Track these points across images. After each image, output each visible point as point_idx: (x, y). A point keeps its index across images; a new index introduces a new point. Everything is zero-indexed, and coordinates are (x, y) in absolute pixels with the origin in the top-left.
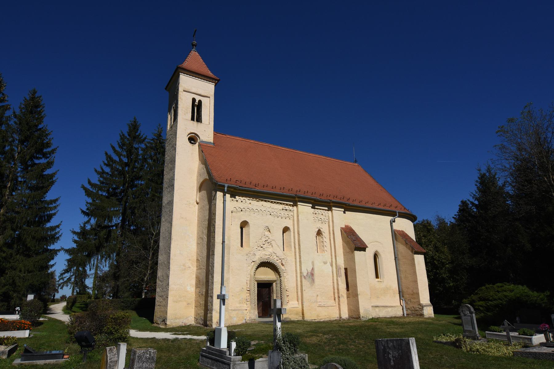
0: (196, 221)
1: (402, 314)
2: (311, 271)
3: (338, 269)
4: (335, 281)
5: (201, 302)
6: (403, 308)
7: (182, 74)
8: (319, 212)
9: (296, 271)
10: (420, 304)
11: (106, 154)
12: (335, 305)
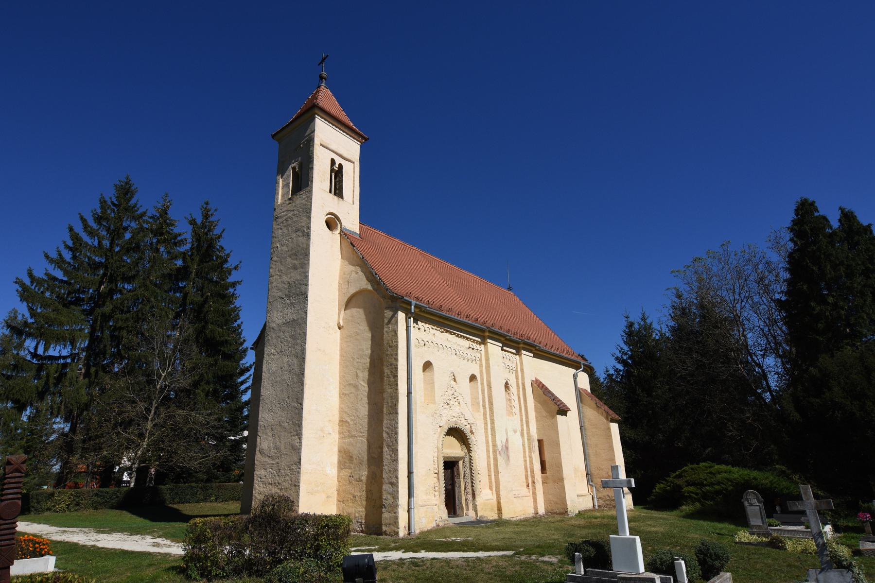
0: (338, 357)
1: (592, 505)
4: (528, 459)
6: (593, 498)
7: (319, 117)
9: (487, 442)
11: (71, 229)
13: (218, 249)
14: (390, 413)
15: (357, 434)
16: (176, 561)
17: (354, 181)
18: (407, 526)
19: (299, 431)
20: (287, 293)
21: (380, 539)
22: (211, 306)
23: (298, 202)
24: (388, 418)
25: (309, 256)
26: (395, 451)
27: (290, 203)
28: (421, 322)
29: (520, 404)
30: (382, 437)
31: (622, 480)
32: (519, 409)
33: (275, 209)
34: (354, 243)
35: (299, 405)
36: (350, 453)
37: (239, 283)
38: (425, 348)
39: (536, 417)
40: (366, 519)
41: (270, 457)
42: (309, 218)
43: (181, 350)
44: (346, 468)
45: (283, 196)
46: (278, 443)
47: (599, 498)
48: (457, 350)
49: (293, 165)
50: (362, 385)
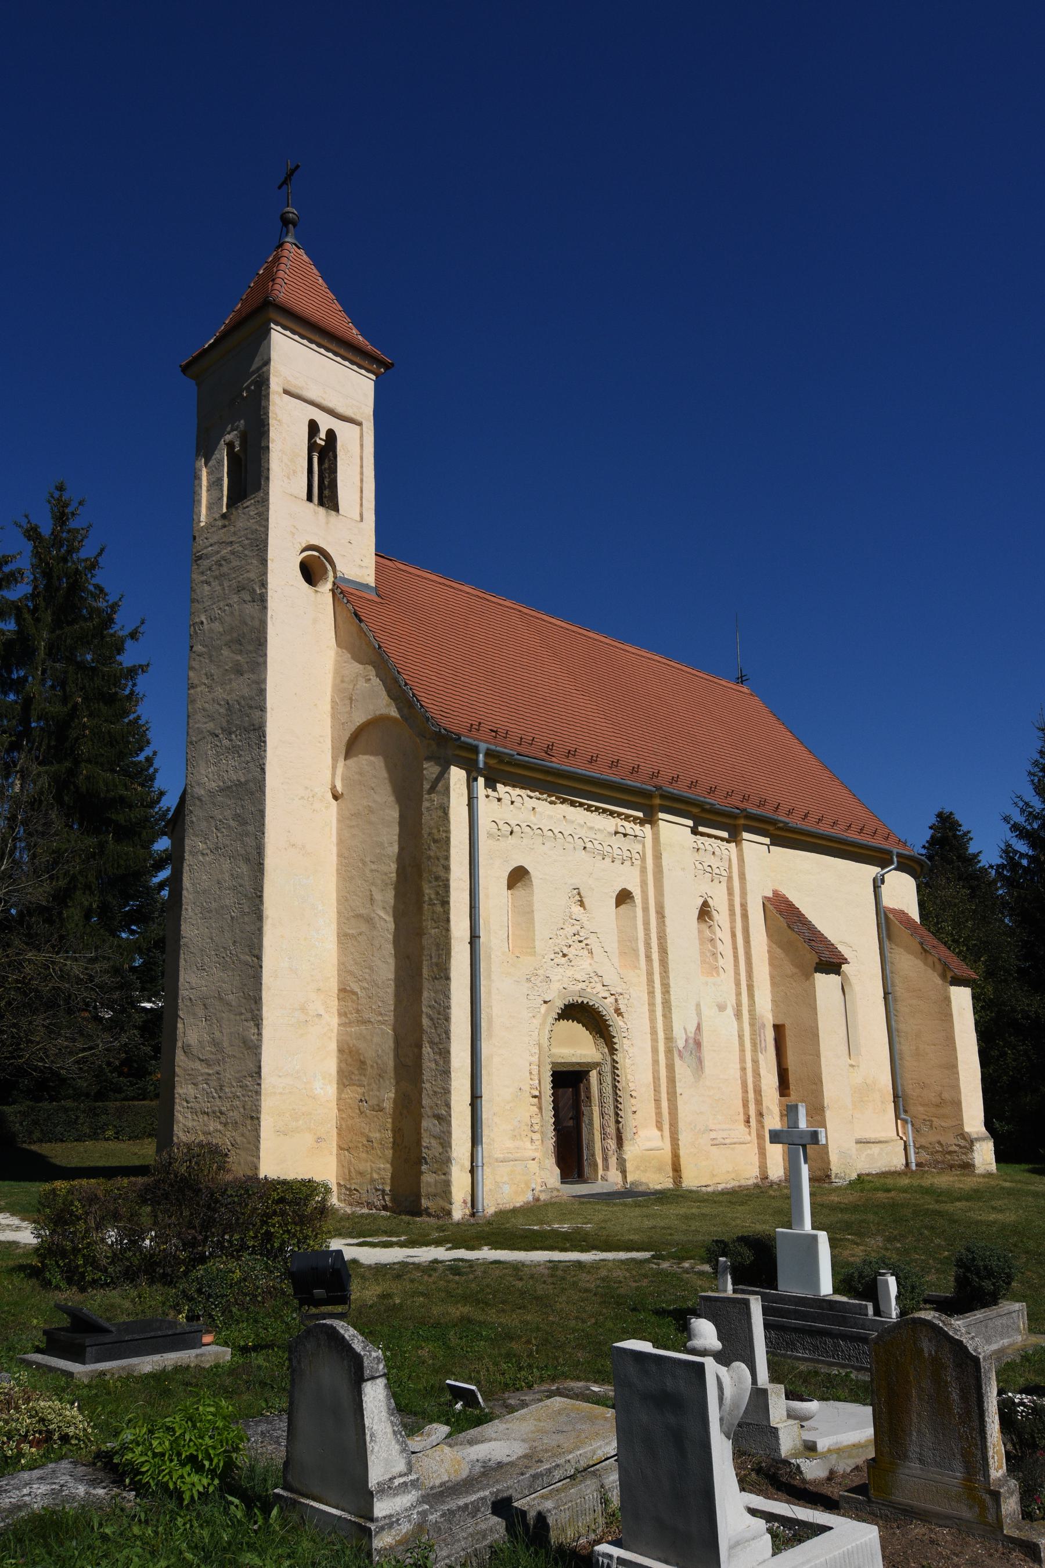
0: (333, 859)
1: (904, 1163)
2: (695, 1033)
3: (760, 1028)
4: (749, 1065)
5: (376, 1135)
7: (279, 328)
8: (707, 844)
9: (654, 1032)
10: (963, 1135)
12: (748, 1138)
13: (91, 593)
14: (436, 978)
15: (374, 1018)
16: (26, 1255)
17: (362, 467)
18: (469, 1199)
19: (256, 1012)
20: (225, 724)
21: (415, 1223)
22: (85, 726)
23: (240, 524)
24: (430, 988)
25: (266, 647)
26: (444, 1054)
27: (224, 526)
28: (503, 784)
29: (735, 948)
30: (420, 1025)
31: (803, 1131)
32: (732, 961)
33: (194, 538)
34: (362, 613)
35: (255, 959)
36: (360, 1054)
37: (144, 668)
38: (512, 840)
39: (772, 978)
40: (392, 1184)
41: (203, 1061)
42: (264, 562)
43: (25, 823)
44: (354, 1085)
45: (209, 508)
46: (217, 1034)
47: (919, 1148)
48: (587, 840)
49: (228, 438)
50: (381, 917)
